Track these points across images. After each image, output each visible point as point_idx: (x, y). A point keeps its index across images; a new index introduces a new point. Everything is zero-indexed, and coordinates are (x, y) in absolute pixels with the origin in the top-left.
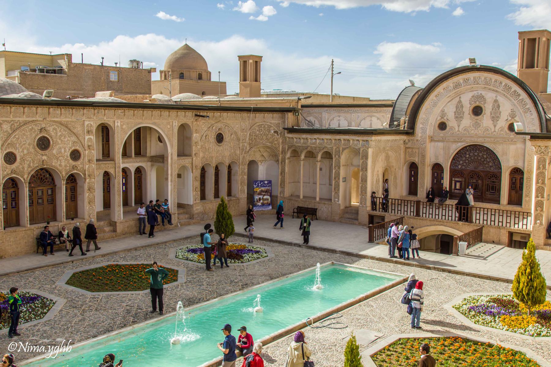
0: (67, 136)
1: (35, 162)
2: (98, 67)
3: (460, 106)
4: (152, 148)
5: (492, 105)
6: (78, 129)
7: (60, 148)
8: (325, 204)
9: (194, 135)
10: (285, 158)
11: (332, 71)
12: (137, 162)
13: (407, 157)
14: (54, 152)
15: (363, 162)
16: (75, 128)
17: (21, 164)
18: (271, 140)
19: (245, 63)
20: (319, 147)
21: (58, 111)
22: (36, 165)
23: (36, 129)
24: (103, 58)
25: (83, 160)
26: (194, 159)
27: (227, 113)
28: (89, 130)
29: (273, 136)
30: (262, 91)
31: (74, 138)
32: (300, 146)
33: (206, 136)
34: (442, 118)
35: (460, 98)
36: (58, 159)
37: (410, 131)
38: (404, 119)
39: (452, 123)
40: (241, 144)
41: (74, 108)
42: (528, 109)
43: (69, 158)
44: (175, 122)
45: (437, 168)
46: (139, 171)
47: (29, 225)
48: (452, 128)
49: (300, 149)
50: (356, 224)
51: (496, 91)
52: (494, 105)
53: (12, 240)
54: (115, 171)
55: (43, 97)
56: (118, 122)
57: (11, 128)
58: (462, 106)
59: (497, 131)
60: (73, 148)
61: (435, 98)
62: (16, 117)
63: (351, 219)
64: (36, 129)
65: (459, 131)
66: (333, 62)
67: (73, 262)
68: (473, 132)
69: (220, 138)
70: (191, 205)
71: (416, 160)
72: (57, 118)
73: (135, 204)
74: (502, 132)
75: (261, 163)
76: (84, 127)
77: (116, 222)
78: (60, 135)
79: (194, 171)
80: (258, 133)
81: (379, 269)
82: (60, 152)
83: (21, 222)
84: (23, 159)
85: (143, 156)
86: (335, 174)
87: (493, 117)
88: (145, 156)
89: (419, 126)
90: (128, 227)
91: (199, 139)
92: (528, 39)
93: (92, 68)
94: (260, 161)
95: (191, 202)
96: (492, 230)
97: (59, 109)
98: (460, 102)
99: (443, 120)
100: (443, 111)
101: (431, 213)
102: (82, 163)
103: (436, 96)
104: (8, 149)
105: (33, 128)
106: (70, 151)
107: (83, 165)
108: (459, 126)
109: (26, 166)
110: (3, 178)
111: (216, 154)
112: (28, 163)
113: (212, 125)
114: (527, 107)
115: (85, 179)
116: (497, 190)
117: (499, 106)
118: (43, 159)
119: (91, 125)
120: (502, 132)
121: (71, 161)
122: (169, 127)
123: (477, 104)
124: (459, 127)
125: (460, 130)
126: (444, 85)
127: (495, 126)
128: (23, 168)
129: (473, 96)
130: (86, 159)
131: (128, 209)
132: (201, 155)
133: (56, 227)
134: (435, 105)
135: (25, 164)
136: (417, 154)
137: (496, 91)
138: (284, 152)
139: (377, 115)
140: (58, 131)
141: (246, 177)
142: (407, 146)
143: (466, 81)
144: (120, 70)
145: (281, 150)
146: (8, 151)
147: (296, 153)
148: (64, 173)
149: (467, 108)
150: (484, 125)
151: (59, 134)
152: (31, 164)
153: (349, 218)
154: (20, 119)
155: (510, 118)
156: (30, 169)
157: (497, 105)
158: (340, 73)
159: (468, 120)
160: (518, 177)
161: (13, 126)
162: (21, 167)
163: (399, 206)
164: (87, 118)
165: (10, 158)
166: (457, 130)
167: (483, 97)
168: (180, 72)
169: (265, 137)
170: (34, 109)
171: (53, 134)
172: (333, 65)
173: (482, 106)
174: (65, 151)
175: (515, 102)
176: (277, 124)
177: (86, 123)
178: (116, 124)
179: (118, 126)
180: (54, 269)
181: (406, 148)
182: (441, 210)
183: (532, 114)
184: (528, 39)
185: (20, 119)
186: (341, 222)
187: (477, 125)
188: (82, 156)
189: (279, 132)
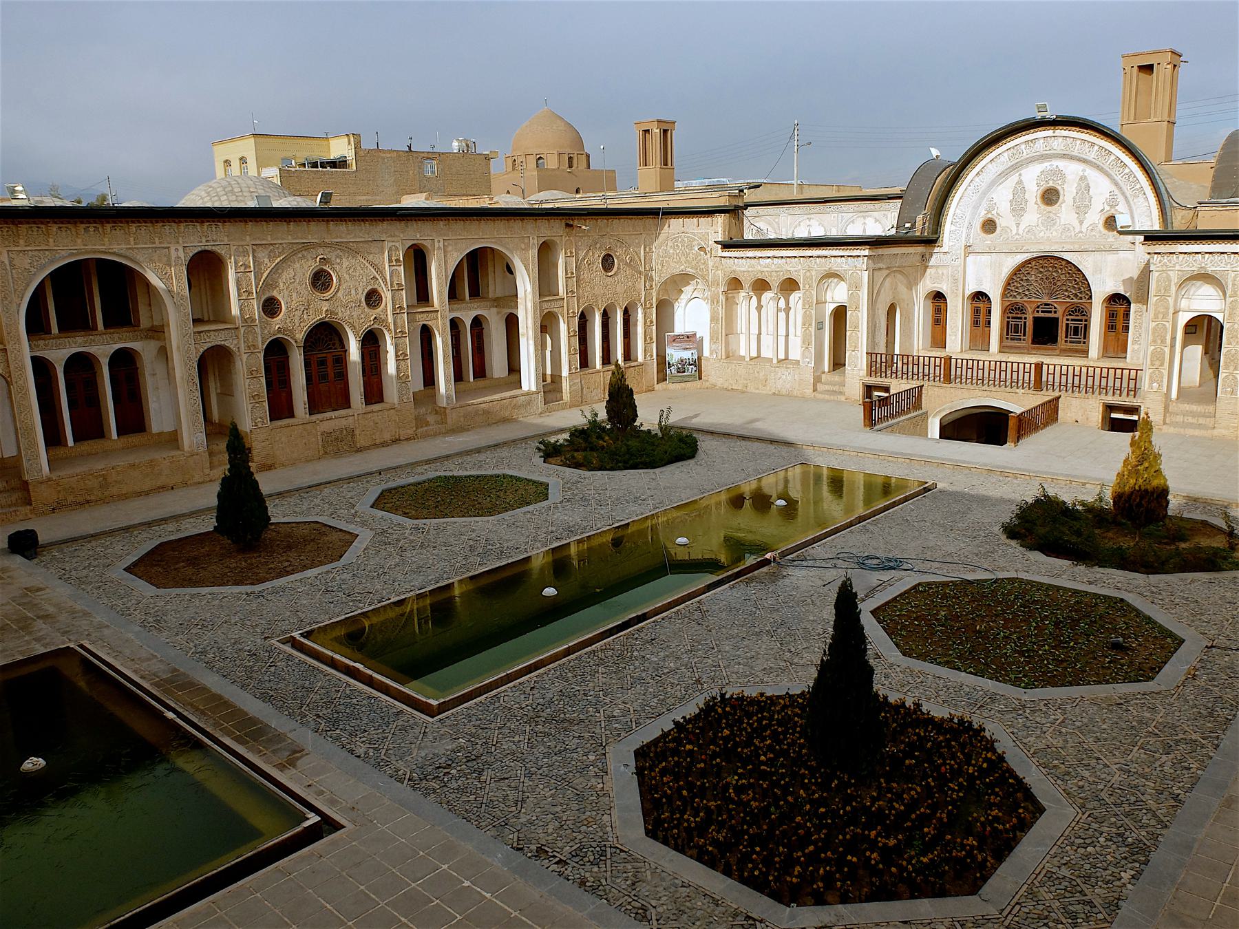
3: (1020, 188)
20: (776, 272)
22: (312, 319)
29: (697, 255)
34: (989, 212)
35: (1020, 175)
44: (177, 250)
48: (1006, 229)
53: (283, 439)
56: (439, 242)
60: (370, 287)
62: (277, 239)
65: (1017, 234)
67: (380, 474)
84: (290, 310)
88: (485, 298)
98: (1020, 182)
108: (1018, 225)
117: (1088, 188)
123: (1051, 184)
125: (1021, 232)
127: (1081, 223)
149: (1033, 192)
155: (1107, 208)
157: (1085, 186)
159: (1034, 212)
169: (683, 259)
173: (1059, 188)
187: (1050, 222)
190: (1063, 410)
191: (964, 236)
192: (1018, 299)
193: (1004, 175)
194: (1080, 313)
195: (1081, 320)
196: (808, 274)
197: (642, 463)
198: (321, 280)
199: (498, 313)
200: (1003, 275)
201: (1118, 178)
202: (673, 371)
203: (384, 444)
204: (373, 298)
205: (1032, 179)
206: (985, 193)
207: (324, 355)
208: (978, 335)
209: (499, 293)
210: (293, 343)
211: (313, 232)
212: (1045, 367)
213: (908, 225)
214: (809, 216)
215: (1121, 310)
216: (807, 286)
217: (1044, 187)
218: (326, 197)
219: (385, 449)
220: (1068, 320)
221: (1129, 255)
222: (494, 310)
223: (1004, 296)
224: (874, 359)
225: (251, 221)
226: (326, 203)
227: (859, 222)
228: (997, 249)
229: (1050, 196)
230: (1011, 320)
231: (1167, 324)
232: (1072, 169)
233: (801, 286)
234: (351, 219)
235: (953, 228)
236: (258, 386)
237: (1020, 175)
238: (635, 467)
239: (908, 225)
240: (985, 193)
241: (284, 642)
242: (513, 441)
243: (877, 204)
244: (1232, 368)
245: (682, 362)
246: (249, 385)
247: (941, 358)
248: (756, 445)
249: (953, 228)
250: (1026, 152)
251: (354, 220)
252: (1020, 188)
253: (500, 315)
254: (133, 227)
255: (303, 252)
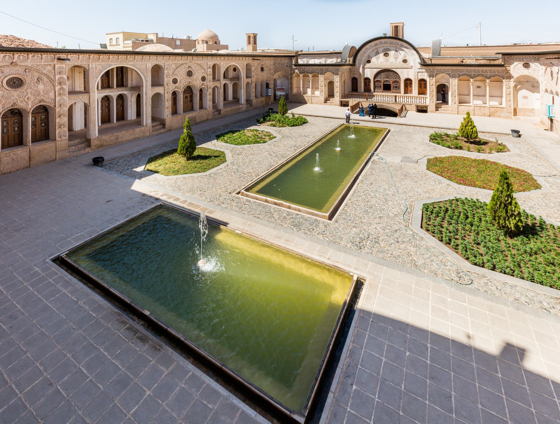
4: (131, 81)
6: (205, 67)
7: (197, 76)
12: (119, 91)
13: (352, 75)
14: (195, 77)
21: (196, 58)
36: (196, 81)
44: (149, 64)
46: (121, 98)
61: (365, 50)
62: (178, 61)
69: (262, 69)
73: (116, 121)
77: (220, 110)
78: (197, 70)
82: (197, 78)
83: (195, 108)
84: (180, 81)
90: (226, 112)
91: (254, 70)
100: (369, 55)
103: (366, 49)
109: (182, 85)
115: (208, 89)
121: (202, 82)
126: (370, 44)
127: (396, 61)
128: (181, 86)
129: (384, 49)
130: (208, 81)
134: (365, 53)
136: (357, 74)
143: (381, 43)
148: (198, 87)
150: (391, 61)
151: (197, 69)
154: (180, 62)
155: (403, 58)
156: (184, 86)
162: (180, 85)
169: (281, 68)
170: (186, 57)
171: (194, 69)
174: (199, 77)
177: (209, 63)
178: (90, 66)
181: (351, 71)
185: (180, 62)
187: (387, 61)
188: (206, 79)
194: (397, 82)
213: (344, 61)
215: (355, 81)
245: (281, 95)
248: (319, 118)
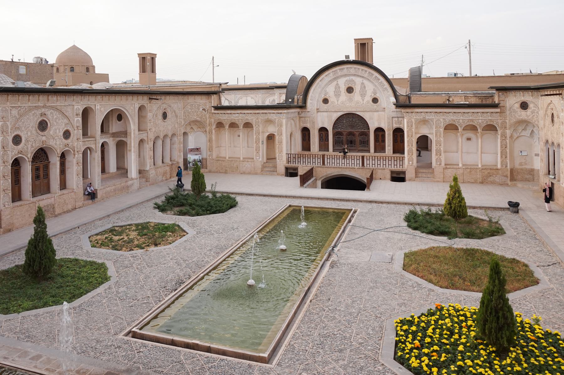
0: (61, 119)
1: (37, 142)
2: (9, 63)
3: (337, 87)
5: (360, 86)
7: (56, 129)
8: (248, 161)
9: (149, 114)
10: (212, 129)
11: (213, 64)
14: (51, 133)
15: (279, 129)
16: (66, 111)
17: (25, 145)
18: (200, 116)
19: (144, 59)
20: (241, 119)
21: (55, 98)
22: (38, 145)
23: (38, 114)
24: (13, 55)
25: (73, 138)
26: (149, 133)
27: (143, 96)
28: (78, 113)
29: (201, 112)
30: (157, 80)
31: (66, 121)
32: (225, 119)
33: (156, 114)
34: (325, 95)
35: (337, 81)
37: (303, 106)
38: (298, 98)
39: (332, 99)
40: (178, 120)
41: (66, 95)
42: (386, 88)
43: (62, 137)
45: (323, 131)
47: (31, 199)
48: (333, 102)
49: (225, 121)
50: (275, 175)
51: (363, 77)
52: (361, 86)
53: (18, 213)
54: (96, 146)
55: (47, 86)
56: (98, 106)
57: (18, 114)
58: (339, 87)
59: (364, 103)
60: (65, 129)
62: (22, 104)
63: (270, 171)
64: (38, 114)
65: (338, 104)
66: (213, 58)
67: (79, 228)
68: (348, 104)
70: (147, 171)
71: (308, 126)
72: (54, 103)
74: (368, 104)
75: (191, 134)
76: (74, 110)
79: (149, 142)
80: (190, 110)
81: (281, 207)
84: (27, 141)
85: (105, 133)
86: (256, 139)
87: (361, 94)
88: (107, 133)
89: (309, 101)
92: (360, 44)
93: (4, 63)
94: (190, 132)
95: (148, 168)
96: (379, 171)
97: (56, 96)
98: (337, 84)
99: (326, 97)
101: (348, 163)
102: (72, 142)
104: (15, 132)
105: (35, 113)
106: (63, 132)
107: (73, 143)
108: (338, 101)
109: (29, 146)
110: (12, 158)
111: (163, 128)
112: (31, 144)
113: (160, 106)
114: (385, 87)
116: (367, 143)
117: (365, 87)
118: (43, 140)
119: (79, 108)
120: (368, 104)
121: (64, 140)
122: (132, 108)
123: (350, 85)
124: (338, 101)
125: (339, 103)
127: (363, 100)
130: (75, 138)
131: (105, 176)
132: (154, 130)
133: (53, 198)
135: (28, 144)
137: (363, 77)
138: (210, 124)
139: (252, 95)
140: (54, 114)
141: (182, 145)
142: (301, 116)
144: (27, 65)
145: (208, 123)
146: (13, 135)
147: (220, 125)
149: (343, 89)
151: (55, 117)
152: (34, 145)
153: (268, 171)
155: (373, 95)
157: (363, 86)
158: (218, 66)
159: (344, 96)
160: (380, 134)
161: (20, 112)
162: (26, 147)
163: (299, 159)
164: (76, 103)
165: (17, 140)
166: (336, 103)
167: (353, 81)
168: (71, 66)
169: (195, 114)
172: (213, 60)
173: (353, 87)
174: (59, 132)
175: (377, 84)
176: (204, 104)
179: (98, 109)
180: (68, 236)
182: (346, 159)
183: (388, 92)
184: (360, 44)
186: (262, 174)
187: (351, 100)
188: (72, 135)
189: (206, 110)
190: (375, 174)
191: (316, 105)
192: (339, 130)
193: (331, 81)
195: (365, 138)
196: (257, 120)
197: (217, 210)
198: (43, 126)
199: (113, 140)
200: (333, 120)
201: (377, 84)
202: (191, 165)
203: (68, 211)
204: (67, 135)
205: (343, 83)
206: (323, 88)
207: (38, 165)
208: (324, 146)
209: (114, 131)
210: (27, 160)
211: (42, 100)
212: (326, 156)
213: (290, 100)
214: (246, 95)
216: (257, 126)
217: (347, 86)
218: (52, 83)
219: (68, 214)
220: (360, 138)
221: (383, 113)
222: (111, 139)
223: (333, 129)
224: (289, 156)
225: (11, 94)
226: (51, 86)
227: (244, 98)
228: (330, 110)
229: (350, 90)
230: (336, 138)
231: (413, 139)
232: (358, 80)
233: (254, 126)
234: (59, 94)
235: (311, 101)
236: (7, 184)
237: (337, 81)
238: (214, 213)
239: (290, 100)
240: (323, 88)
241: (127, 335)
242: (137, 204)
243: (252, 91)
244: (439, 155)
245: (195, 160)
246: (3, 184)
247: (359, 156)
249: (311, 101)
250: (340, 73)
251: (61, 95)
252: (337, 87)
253: (115, 141)
254: (10, 97)
255: (35, 111)
